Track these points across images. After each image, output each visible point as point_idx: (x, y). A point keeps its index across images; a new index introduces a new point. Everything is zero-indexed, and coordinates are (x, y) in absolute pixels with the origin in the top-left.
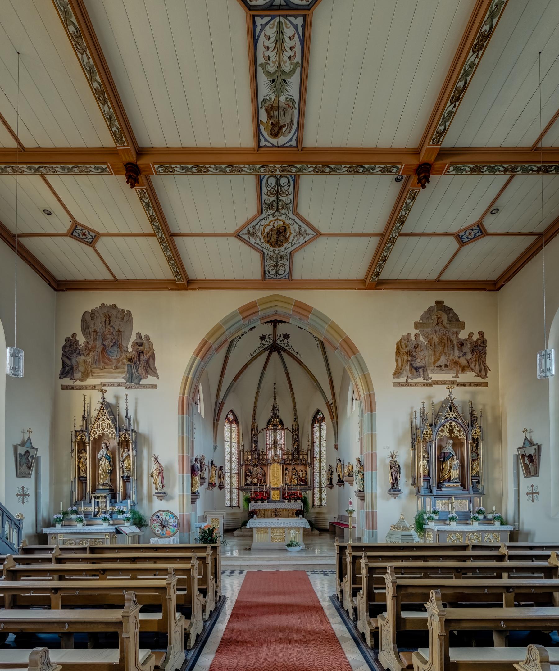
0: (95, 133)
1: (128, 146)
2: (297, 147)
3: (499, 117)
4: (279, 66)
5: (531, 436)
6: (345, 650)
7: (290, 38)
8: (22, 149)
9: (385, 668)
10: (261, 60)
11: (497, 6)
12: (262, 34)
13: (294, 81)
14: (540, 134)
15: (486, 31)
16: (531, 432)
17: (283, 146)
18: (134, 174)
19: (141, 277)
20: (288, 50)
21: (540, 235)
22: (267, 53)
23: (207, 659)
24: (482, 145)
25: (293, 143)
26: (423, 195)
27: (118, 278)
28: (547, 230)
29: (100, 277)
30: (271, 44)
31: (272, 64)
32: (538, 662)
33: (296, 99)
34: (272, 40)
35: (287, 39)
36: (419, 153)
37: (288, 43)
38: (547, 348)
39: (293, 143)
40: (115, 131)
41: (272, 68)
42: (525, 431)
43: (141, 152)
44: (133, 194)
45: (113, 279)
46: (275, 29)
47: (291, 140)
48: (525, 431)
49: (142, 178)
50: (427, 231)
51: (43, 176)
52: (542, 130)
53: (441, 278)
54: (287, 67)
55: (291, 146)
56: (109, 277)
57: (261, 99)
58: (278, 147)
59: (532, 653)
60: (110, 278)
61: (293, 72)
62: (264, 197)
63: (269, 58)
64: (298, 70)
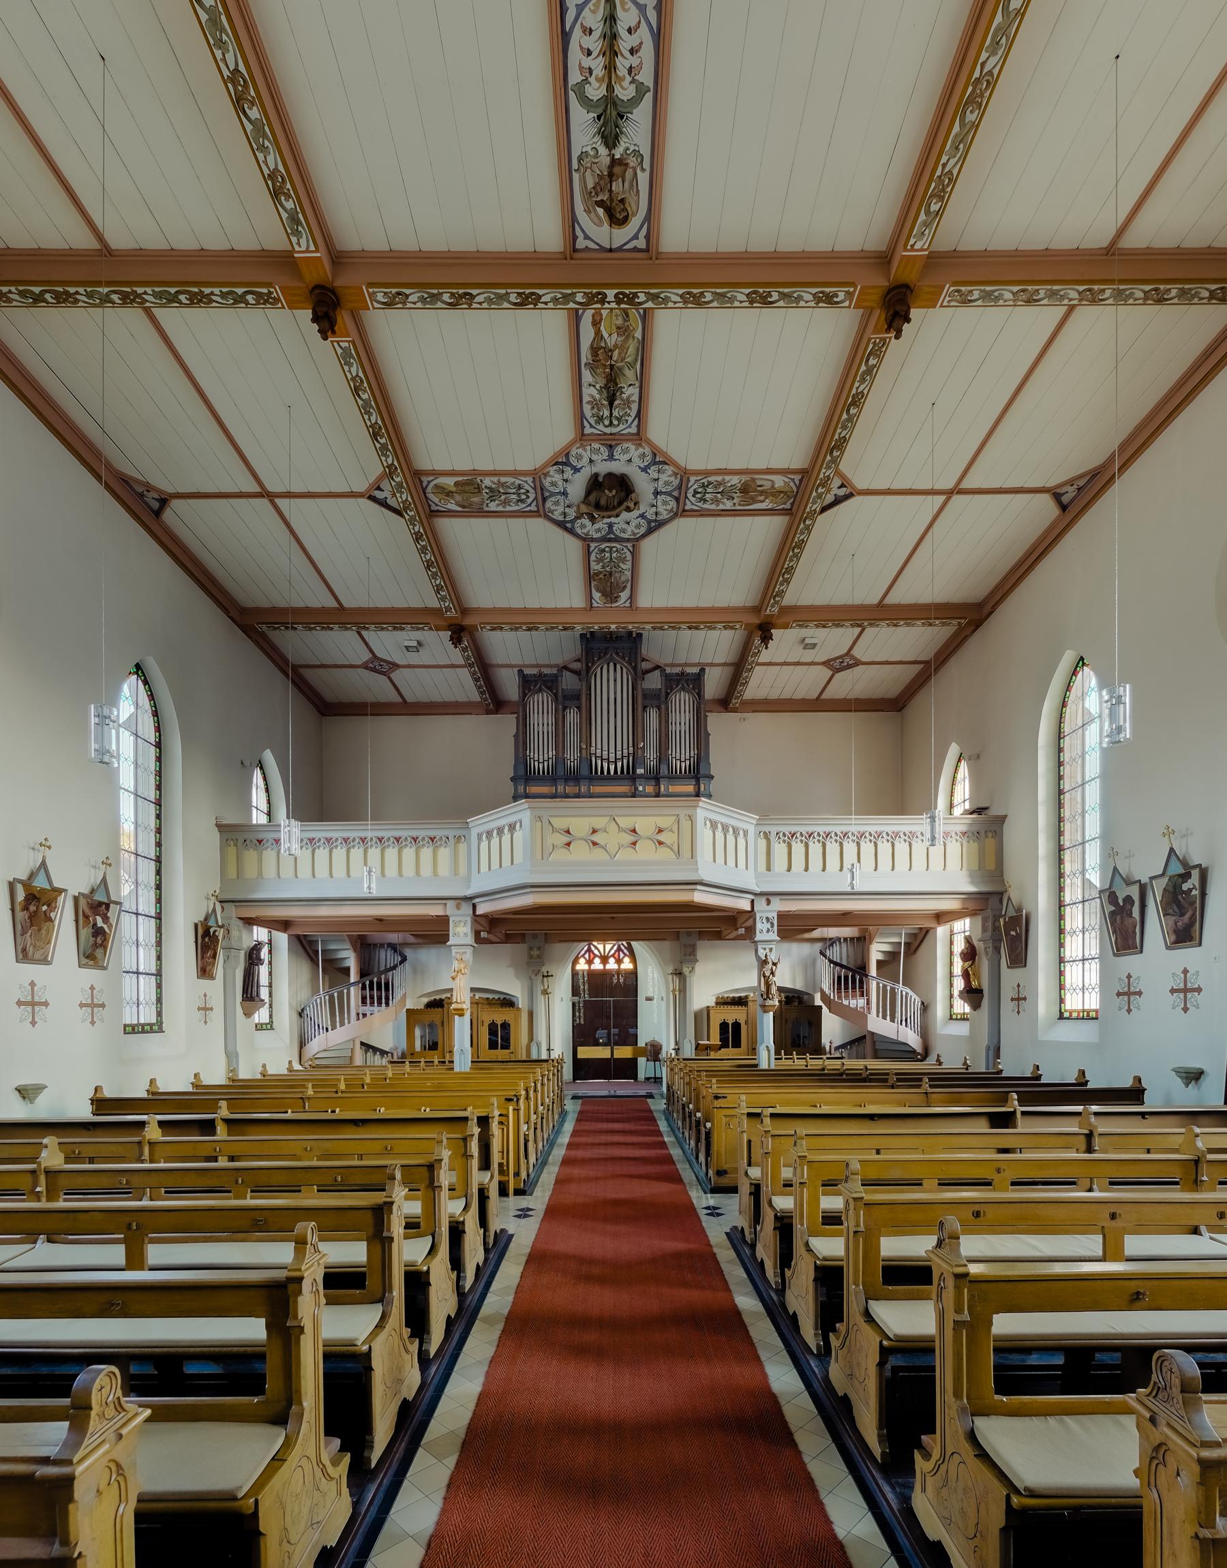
0: (253, 223)
1: (317, 250)
2: (647, 250)
3: (1044, 174)
4: (610, 88)
5: (1187, 846)
6: (763, 1359)
7: (630, 31)
8: (106, 251)
9: (840, 1394)
10: (575, 77)
11: (957, 148)
12: (578, 25)
13: (641, 116)
14: (1114, 232)
15: (972, 112)
16: (1129, 856)
17: (620, 249)
18: (328, 307)
19: (437, 698)
20: (627, 54)
21: (927, 663)
22: (587, 62)
23: (418, 1509)
24: (825, 602)
25: (641, 243)
26: (895, 347)
27: (345, 605)
28: (937, 655)
29: (383, 699)
30: (595, 43)
31: (595, 84)
32: (1176, 1391)
33: (646, 151)
34: (597, 34)
35: (623, 32)
36: (889, 262)
37: (626, 42)
38: (936, 808)
39: (641, 243)
40: (287, 200)
41: (596, 91)
42: (1169, 832)
43: (339, 259)
44: (325, 351)
45: (336, 605)
46: (600, 14)
47: (636, 237)
48: (1169, 832)
49: (344, 318)
50: (873, 487)
51: (148, 311)
52: (1119, 224)
53: (886, 601)
54: (625, 92)
55: (636, 250)
56: (396, 698)
57: (575, 154)
58: (611, 250)
59: (1164, 1370)
60: (85, 241)
61: (636, 101)
62: (593, 564)
63: (591, 71)
64: (649, 97)
